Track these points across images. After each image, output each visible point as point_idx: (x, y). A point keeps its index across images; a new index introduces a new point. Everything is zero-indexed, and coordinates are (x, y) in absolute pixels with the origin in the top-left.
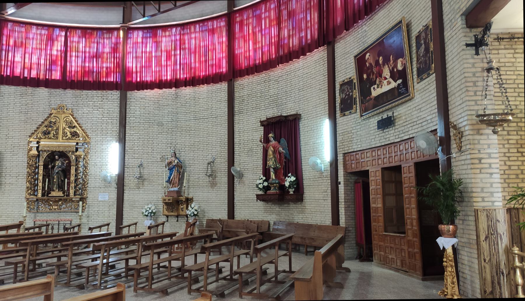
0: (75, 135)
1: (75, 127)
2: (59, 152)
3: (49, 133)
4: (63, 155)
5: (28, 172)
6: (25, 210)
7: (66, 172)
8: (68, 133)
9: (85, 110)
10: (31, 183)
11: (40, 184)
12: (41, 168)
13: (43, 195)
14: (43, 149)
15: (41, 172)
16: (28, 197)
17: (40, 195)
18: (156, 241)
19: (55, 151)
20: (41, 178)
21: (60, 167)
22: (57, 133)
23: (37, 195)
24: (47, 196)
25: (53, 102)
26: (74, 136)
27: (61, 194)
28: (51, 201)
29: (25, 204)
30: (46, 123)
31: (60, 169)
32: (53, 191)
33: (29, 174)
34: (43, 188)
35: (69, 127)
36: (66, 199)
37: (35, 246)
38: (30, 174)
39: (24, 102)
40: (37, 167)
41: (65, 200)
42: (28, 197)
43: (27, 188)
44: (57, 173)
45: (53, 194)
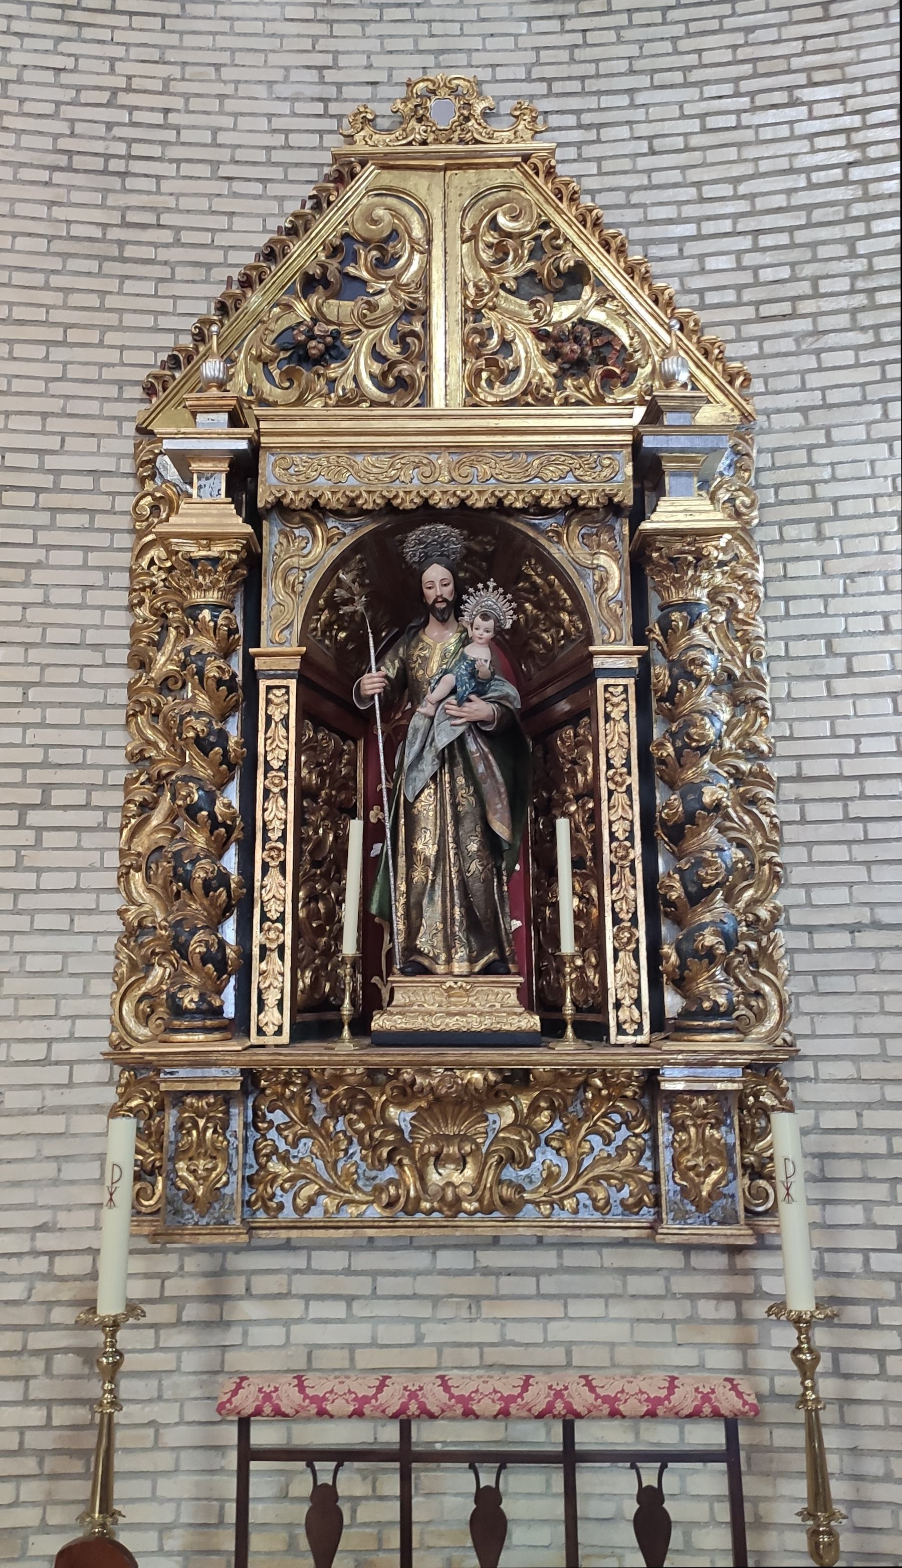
0: (587, 357)
1: (577, 277)
2: (462, 514)
3: (335, 351)
4: (496, 542)
5: (138, 758)
6: (117, 1223)
7: (532, 748)
8: (527, 348)
9: (667, 111)
10: (177, 882)
11: (276, 891)
12: (281, 703)
13: (314, 1018)
14: (295, 498)
15: (279, 745)
16: (144, 1039)
17: (273, 1019)
18: (237, 841)
19: (427, 512)
20: (277, 814)
21: (481, 689)
22: (413, 344)
23: (240, 1025)
24: (361, 1026)
25: (352, 69)
26: (577, 367)
27: (498, 1005)
28: (405, 1094)
29: (122, 1140)
30: (304, 254)
31: (480, 709)
32: (417, 966)
33: (151, 780)
34: (314, 935)
35: (531, 285)
36: (559, 1068)
37: (194, 466)
38: (159, 783)
39: (94, 72)
40: (243, 695)
41: (567, 1094)
42: (144, 1039)
43: (135, 932)
44: (453, 754)
45: (413, 1006)
